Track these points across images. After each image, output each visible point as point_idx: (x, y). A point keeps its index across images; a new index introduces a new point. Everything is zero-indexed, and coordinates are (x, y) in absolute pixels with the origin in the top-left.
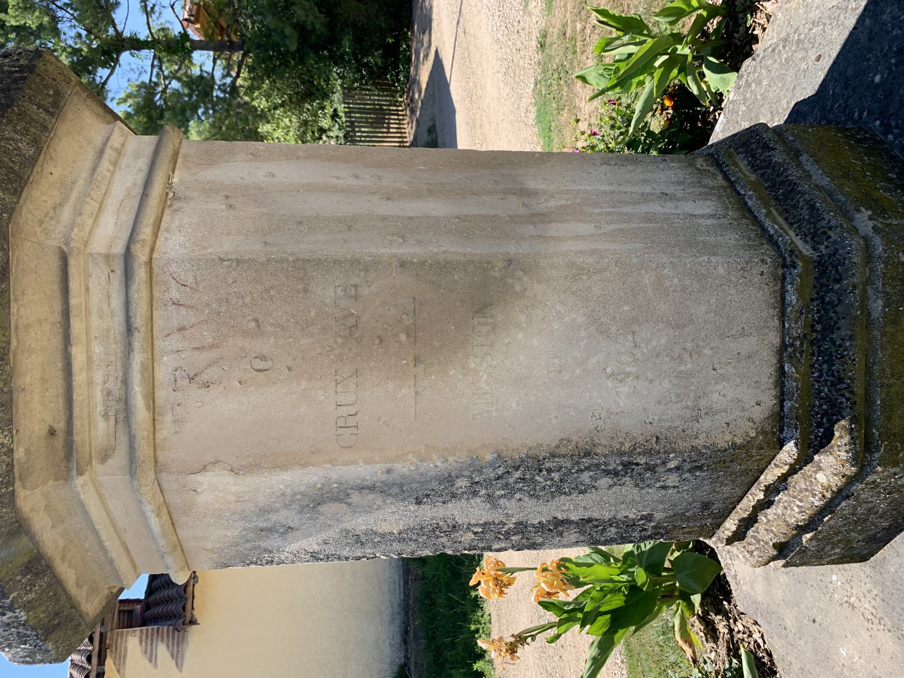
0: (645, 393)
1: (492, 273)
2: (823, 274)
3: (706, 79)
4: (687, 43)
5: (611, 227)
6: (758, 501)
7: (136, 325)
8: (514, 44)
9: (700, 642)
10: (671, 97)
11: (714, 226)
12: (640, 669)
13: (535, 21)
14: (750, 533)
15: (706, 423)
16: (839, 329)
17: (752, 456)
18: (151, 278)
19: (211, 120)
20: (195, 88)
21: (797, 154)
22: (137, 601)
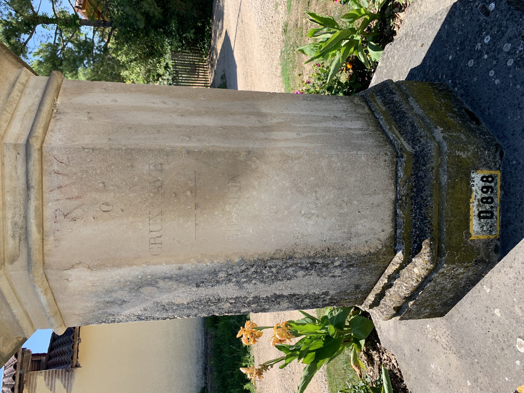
0: (322, 224)
1: (239, 158)
2: (417, 161)
3: (369, 54)
4: (358, 34)
5: (306, 134)
6: (385, 284)
7: (32, 185)
8: (270, 29)
9: (364, 366)
10: (351, 63)
11: (361, 135)
12: (335, 383)
13: (281, 17)
14: (382, 302)
15: (354, 241)
16: (425, 191)
17: (380, 259)
18: (42, 158)
19: (92, 67)
20: (82, 47)
21: (407, 97)
22: (44, 355)
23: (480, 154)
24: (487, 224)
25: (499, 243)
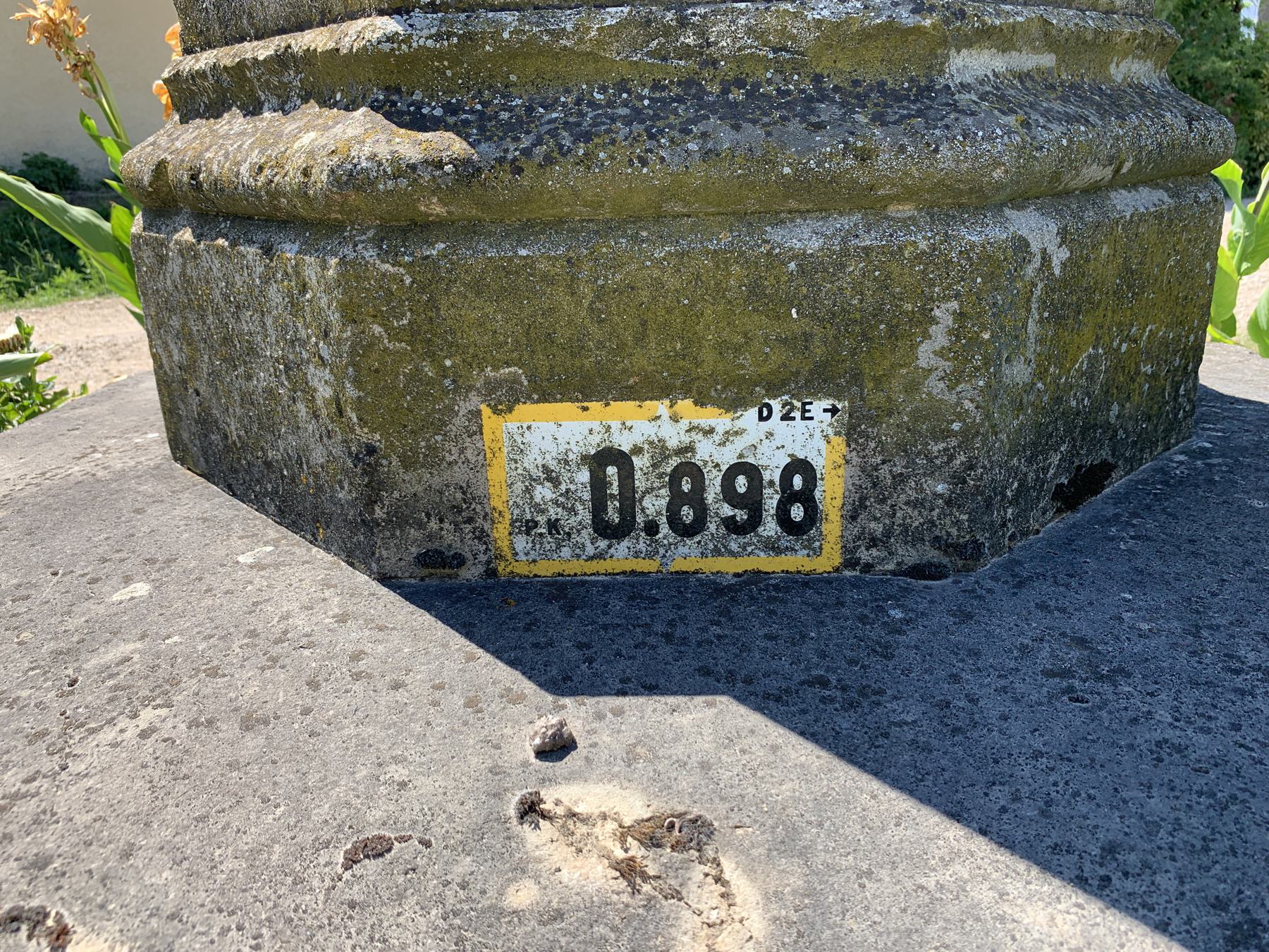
23: (935, 448)
24: (567, 501)
25: (471, 573)
